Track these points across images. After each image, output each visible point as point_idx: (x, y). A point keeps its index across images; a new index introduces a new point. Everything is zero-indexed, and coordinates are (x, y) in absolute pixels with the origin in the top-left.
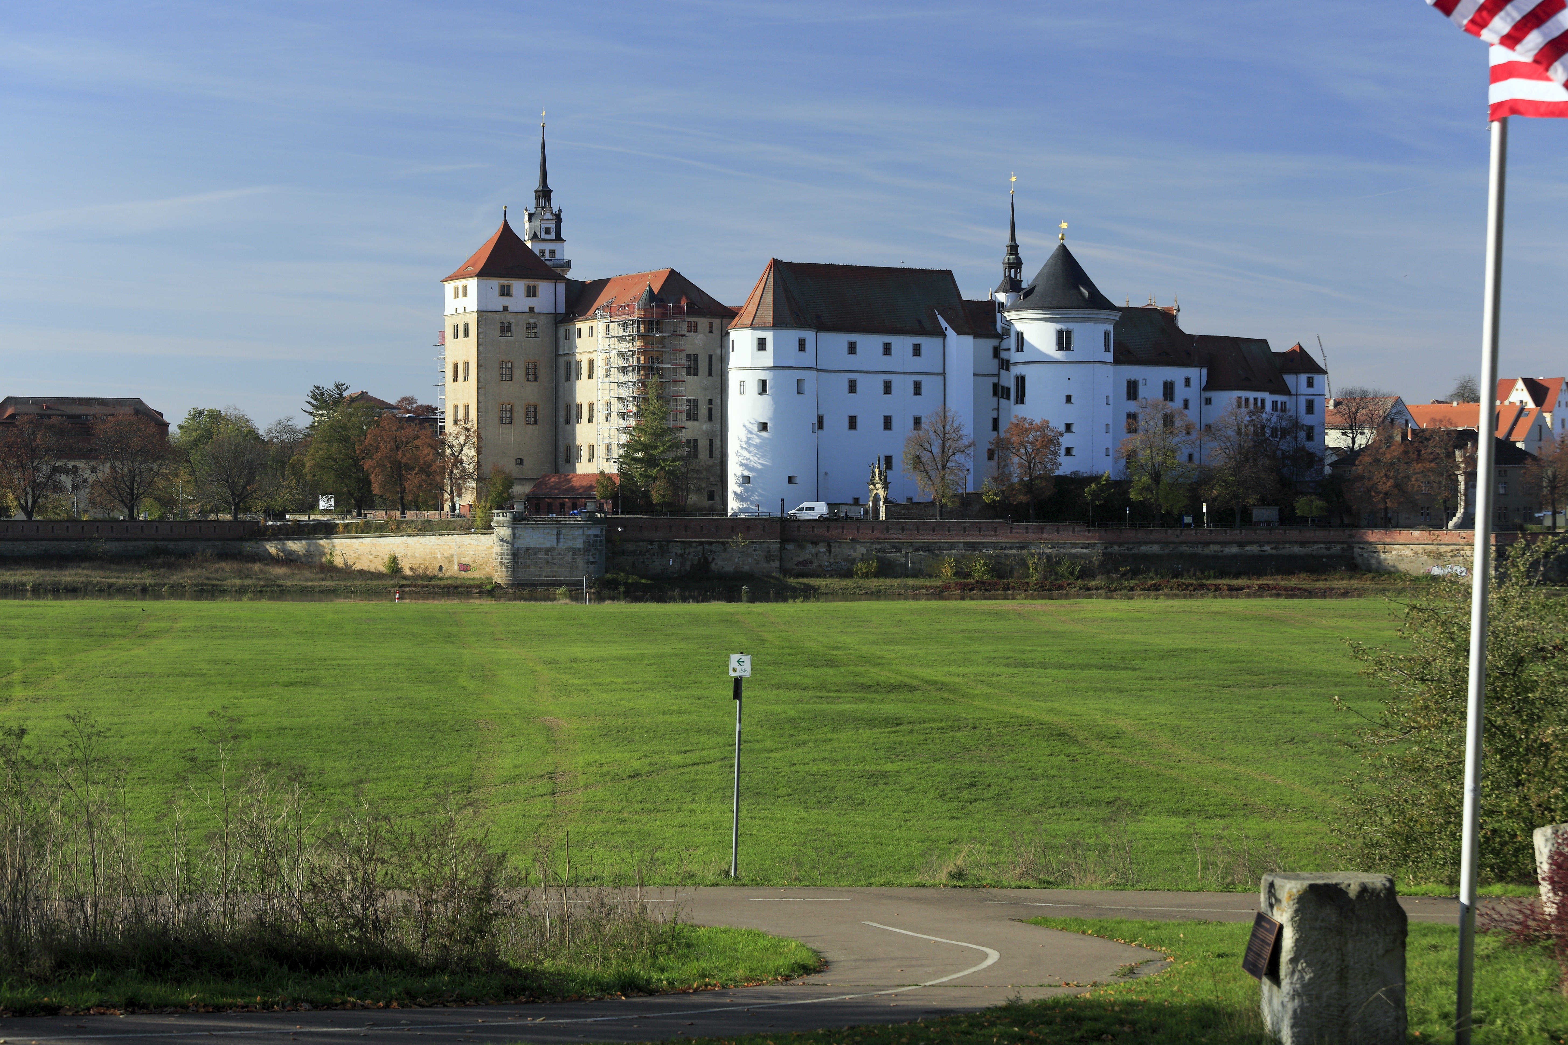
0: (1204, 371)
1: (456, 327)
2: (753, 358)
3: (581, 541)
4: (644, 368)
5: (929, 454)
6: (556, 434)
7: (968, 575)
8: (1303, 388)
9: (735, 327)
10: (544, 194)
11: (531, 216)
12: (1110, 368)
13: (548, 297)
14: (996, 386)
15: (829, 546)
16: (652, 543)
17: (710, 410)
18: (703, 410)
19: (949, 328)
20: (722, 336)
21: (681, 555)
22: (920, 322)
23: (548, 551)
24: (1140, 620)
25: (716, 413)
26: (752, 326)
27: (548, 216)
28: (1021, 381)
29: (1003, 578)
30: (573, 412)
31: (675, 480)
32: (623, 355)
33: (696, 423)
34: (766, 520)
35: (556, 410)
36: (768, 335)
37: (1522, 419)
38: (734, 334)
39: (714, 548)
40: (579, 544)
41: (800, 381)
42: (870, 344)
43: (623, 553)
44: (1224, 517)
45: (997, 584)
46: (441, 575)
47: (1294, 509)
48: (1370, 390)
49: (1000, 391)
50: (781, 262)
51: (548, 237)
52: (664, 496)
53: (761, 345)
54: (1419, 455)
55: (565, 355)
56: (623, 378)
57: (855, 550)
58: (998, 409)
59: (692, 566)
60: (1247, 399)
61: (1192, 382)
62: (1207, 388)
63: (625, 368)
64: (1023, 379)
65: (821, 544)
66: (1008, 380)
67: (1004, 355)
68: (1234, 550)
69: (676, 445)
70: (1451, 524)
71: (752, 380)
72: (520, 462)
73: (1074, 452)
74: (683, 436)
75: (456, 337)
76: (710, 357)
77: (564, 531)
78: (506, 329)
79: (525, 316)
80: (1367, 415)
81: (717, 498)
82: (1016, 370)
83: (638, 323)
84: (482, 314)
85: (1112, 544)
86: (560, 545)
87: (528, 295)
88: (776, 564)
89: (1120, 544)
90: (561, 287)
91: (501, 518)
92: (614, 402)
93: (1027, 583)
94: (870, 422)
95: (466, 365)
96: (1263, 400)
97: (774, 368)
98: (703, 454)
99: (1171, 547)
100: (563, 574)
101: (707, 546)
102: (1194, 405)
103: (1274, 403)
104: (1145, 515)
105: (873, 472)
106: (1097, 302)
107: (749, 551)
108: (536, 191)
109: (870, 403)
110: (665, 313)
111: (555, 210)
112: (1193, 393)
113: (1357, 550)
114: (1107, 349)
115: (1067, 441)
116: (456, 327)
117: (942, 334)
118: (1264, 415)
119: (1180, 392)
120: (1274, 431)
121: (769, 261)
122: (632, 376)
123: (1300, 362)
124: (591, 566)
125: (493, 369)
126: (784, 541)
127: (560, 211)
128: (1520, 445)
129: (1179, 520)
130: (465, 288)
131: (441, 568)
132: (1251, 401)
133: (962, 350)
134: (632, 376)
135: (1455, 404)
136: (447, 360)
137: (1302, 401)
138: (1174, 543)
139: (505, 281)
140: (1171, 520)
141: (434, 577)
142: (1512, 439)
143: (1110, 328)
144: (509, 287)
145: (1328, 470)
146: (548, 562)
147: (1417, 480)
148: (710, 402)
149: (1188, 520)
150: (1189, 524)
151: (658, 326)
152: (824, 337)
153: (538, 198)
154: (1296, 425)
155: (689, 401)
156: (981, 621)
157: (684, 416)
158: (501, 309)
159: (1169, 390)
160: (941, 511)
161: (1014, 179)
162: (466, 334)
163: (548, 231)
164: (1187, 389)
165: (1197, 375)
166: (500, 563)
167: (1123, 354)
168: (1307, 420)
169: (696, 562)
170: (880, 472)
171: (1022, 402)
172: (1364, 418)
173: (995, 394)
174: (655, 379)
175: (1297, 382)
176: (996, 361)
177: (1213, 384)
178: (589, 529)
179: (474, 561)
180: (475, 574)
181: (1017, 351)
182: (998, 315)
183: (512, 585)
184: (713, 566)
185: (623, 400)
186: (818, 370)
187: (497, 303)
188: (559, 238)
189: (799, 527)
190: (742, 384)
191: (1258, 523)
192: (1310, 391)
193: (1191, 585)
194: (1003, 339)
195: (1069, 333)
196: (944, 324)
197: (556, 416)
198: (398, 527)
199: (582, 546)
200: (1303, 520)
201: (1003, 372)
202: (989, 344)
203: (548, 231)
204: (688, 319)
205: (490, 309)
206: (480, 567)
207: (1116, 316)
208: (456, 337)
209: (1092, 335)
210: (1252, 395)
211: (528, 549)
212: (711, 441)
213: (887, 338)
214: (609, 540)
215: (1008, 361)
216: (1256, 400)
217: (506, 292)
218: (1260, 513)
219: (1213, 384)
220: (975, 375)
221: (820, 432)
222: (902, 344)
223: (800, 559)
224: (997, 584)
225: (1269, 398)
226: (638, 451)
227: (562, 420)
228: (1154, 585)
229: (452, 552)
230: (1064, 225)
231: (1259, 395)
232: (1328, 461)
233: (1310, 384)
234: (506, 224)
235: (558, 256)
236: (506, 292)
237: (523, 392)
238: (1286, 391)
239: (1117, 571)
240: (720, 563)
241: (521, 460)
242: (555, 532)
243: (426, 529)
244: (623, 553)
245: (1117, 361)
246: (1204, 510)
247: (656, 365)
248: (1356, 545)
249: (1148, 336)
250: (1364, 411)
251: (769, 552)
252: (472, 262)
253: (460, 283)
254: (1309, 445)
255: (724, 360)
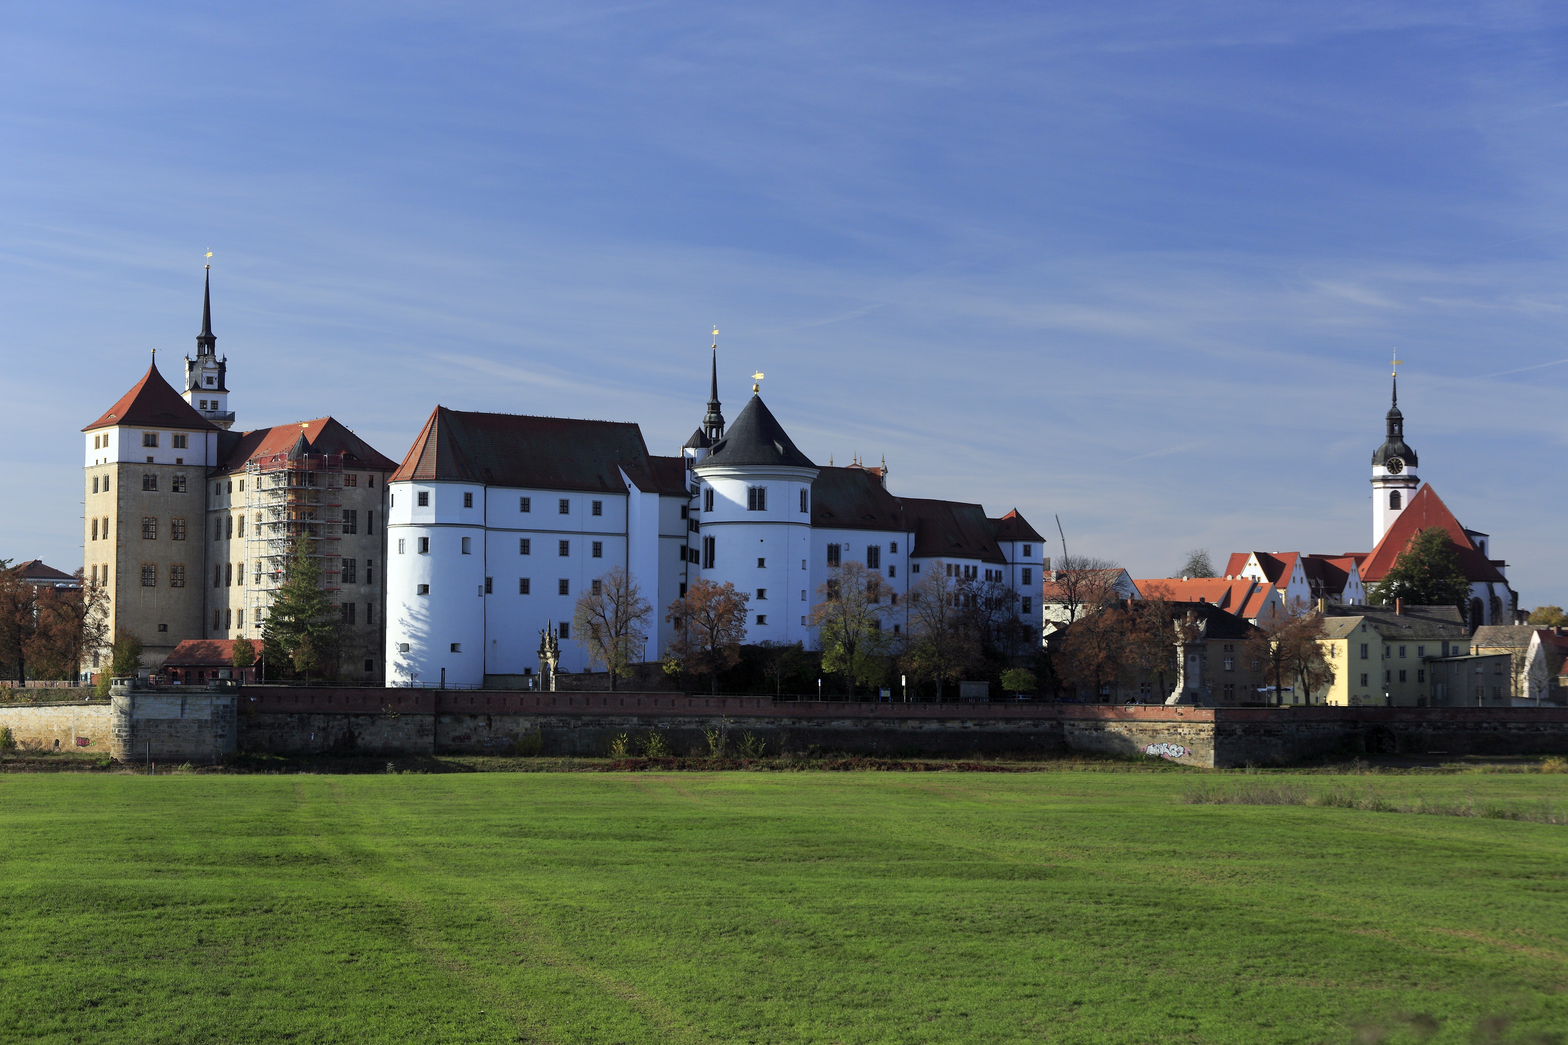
0: (912, 536)
1: (96, 480)
2: (414, 513)
3: (209, 712)
4: (295, 524)
5: (602, 619)
6: (205, 597)
7: (642, 751)
8: (1020, 556)
9: (395, 481)
10: (207, 341)
11: (192, 365)
12: (808, 530)
13: (198, 447)
14: (684, 549)
15: (489, 719)
16: (291, 715)
17: (370, 571)
18: (361, 573)
19: (633, 485)
20: (383, 492)
21: (324, 729)
22: (600, 478)
23: (171, 722)
24: (772, 793)
25: (376, 576)
26: (413, 479)
27: (210, 364)
28: (710, 542)
29: (680, 755)
30: (223, 574)
31: (325, 648)
32: (274, 510)
33: (353, 586)
34: (419, 690)
35: (205, 571)
36: (431, 491)
37: (1254, 595)
38: (394, 488)
39: (360, 720)
40: (206, 715)
41: (465, 540)
42: (545, 501)
43: (259, 726)
44: (924, 691)
45: (671, 762)
46: (57, 750)
47: (1000, 683)
48: (1090, 559)
49: (688, 555)
50: (446, 410)
51: (210, 387)
52: (308, 663)
53: (423, 499)
54: (1134, 624)
55: (215, 511)
56: (273, 536)
57: (518, 725)
58: (686, 574)
59: (336, 741)
60: (958, 567)
61: (899, 548)
62: (914, 555)
63: (275, 524)
64: (712, 540)
65: (481, 718)
66: (697, 543)
67: (693, 515)
68: (934, 726)
69: (330, 609)
70: (1170, 701)
71: (412, 537)
72: (164, 628)
73: (767, 621)
74: (338, 600)
75: (96, 491)
76: (370, 513)
77: (189, 701)
78: (149, 483)
79: (171, 469)
80: (1086, 585)
81: (375, 668)
82: (706, 532)
83: (289, 475)
84: (122, 464)
85: (800, 719)
86: (186, 716)
87: (176, 446)
88: (430, 739)
89: (809, 719)
90: (213, 437)
91: (119, 686)
92: (264, 562)
93: (705, 761)
94: (544, 587)
95: (106, 521)
96: (975, 568)
97: (436, 525)
98: (360, 620)
99: (865, 722)
100: (188, 748)
101: (353, 719)
102: (900, 572)
103: (988, 573)
104: (838, 688)
105: (544, 640)
106: (793, 458)
107: (400, 724)
108: (198, 338)
109: (544, 565)
110: (320, 466)
111: (219, 359)
112: (900, 560)
113: (1067, 727)
114: (804, 509)
115: (755, 608)
116: (96, 480)
117: (626, 492)
118: (974, 584)
119: (886, 558)
120: (988, 602)
121: (433, 409)
122: (282, 534)
123: (1017, 529)
124: (220, 740)
125: (135, 526)
126: (438, 714)
127: (225, 359)
128: (1251, 621)
129: (877, 693)
130: (106, 437)
131: (57, 742)
132: (962, 569)
133: (646, 508)
134: (282, 534)
135: (1185, 579)
136: (87, 517)
137: (1019, 570)
138: (868, 718)
139: (150, 431)
140: (866, 694)
141: (50, 753)
142: (1245, 616)
143: (808, 487)
144: (154, 436)
145: (1045, 643)
146: (171, 735)
147: (1131, 651)
148: (370, 562)
149: (885, 693)
150: (887, 698)
151: (312, 478)
152: (493, 492)
153: (201, 345)
154: (1011, 595)
155: (345, 562)
156: (583, 793)
157: (340, 578)
158: (145, 461)
159: (873, 555)
160: (614, 682)
161: (716, 332)
162: (107, 489)
163: (210, 381)
164: (894, 555)
165: (905, 540)
166: (117, 736)
167: (823, 517)
168: (1023, 591)
169: (340, 736)
170: (551, 639)
171: (712, 566)
172: (1084, 589)
173: (683, 557)
174: (305, 535)
175: (1014, 550)
176: (685, 522)
177: (920, 550)
178: (218, 698)
179: (94, 735)
180: (94, 750)
181: (707, 510)
182: (688, 472)
183: (129, 761)
184: (359, 741)
185: (272, 559)
186: (486, 529)
187: (141, 453)
188: (222, 388)
189: (456, 698)
190: (401, 542)
191: (966, 700)
192: (1027, 559)
193: (885, 764)
194: (692, 498)
195: (762, 491)
196: (627, 480)
197: (205, 578)
198: (12, 697)
199: (209, 718)
200: (1011, 694)
201: (692, 534)
202: (676, 504)
203: (210, 381)
204: (344, 471)
205: (132, 459)
206: (100, 741)
207: (814, 474)
208: (96, 491)
209: (787, 494)
210: (963, 562)
211: (149, 721)
212: (370, 606)
213: (597, 497)
214: (241, 712)
215: (697, 522)
216: (967, 567)
217: (150, 442)
218: (968, 689)
219: (920, 550)
220: (660, 536)
221: (488, 595)
222: (581, 502)
223: (457, 734)
224: (671, 762)
225: (982, 567)
226: (284, 614)
227: (211, 582)
228: (845, 764)
229: (70, 724)
230: (759, 376)
231: (971, 563)
232: (1046, 633)
233: (1027, 552)
234: (154, 369)
235: (220, 408)
236: (150, 442)
237: (165, 551)
238: (1002, 560)
239: (805, 748)
240: (367, 738)
241: (165, 626)
242: (179, 702)
243: (40, 700)
244: (259, 726)
245: (816, 523)
246: (904, 683)
247: (308, 521)
248: (1066, 722)
249: (850, 498)
250: (1084, 582)
251: (422, 725)
252: (115, 410)
253: (101, 432)
254: (1023, 618)
255: (384, 516)
